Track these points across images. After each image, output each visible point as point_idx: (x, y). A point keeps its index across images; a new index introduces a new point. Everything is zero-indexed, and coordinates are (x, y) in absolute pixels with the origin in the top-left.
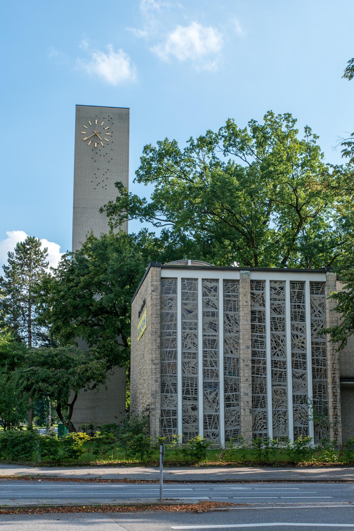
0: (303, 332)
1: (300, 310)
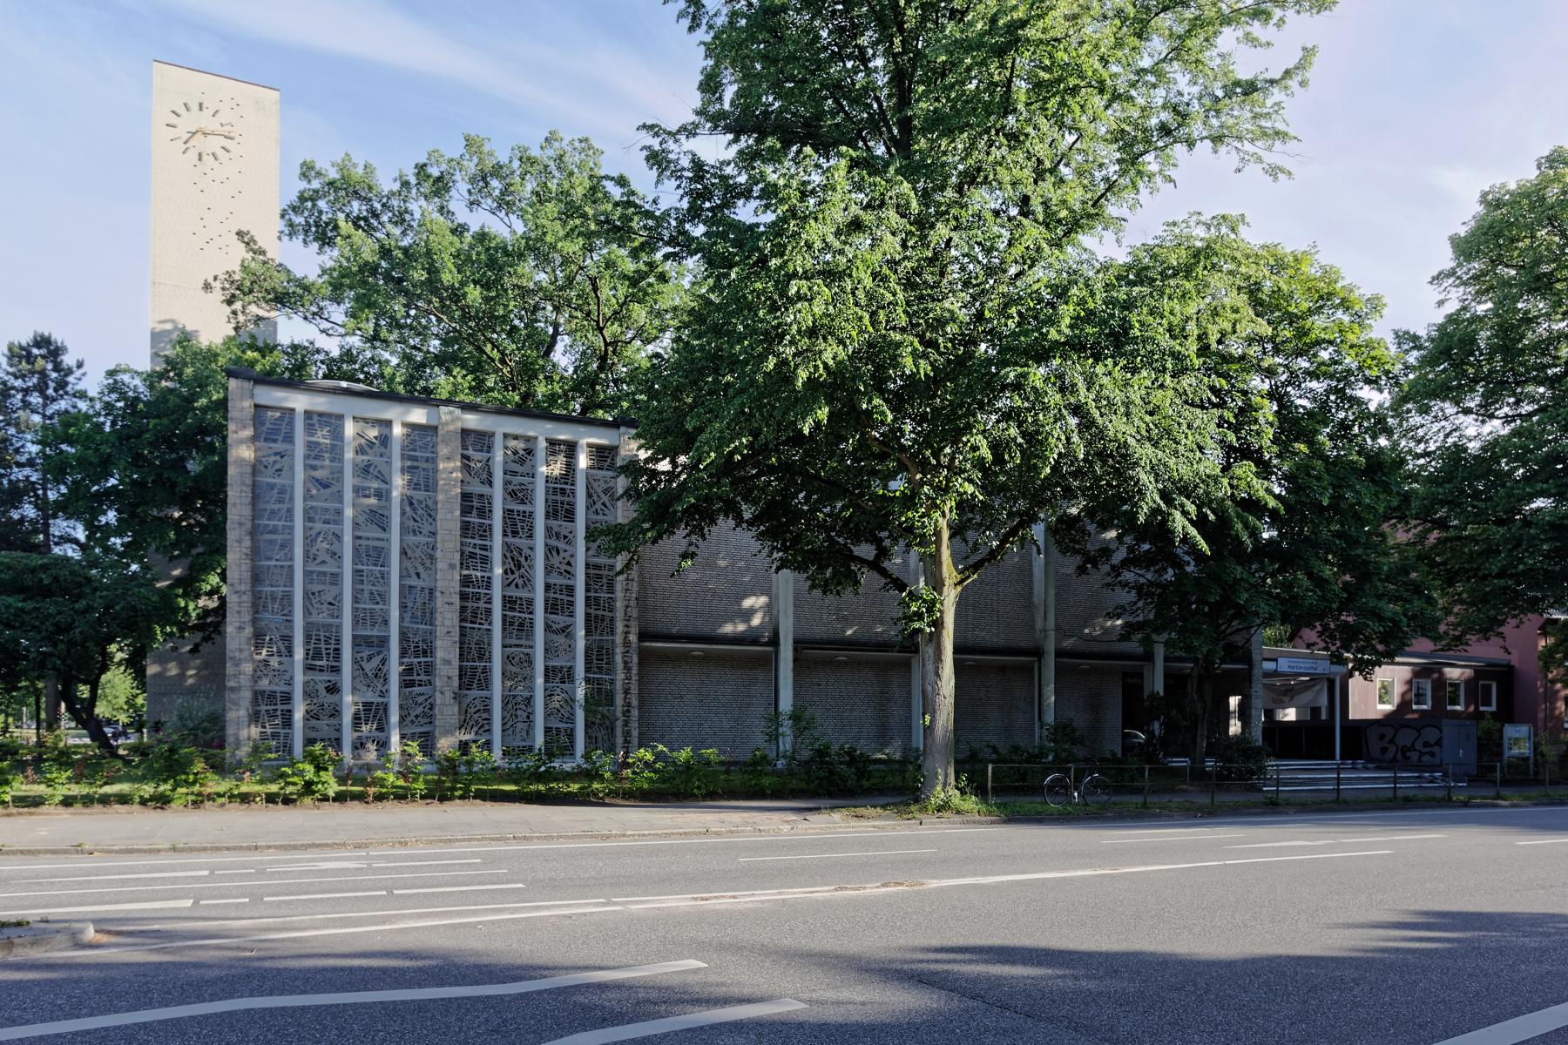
1: (566, 499)
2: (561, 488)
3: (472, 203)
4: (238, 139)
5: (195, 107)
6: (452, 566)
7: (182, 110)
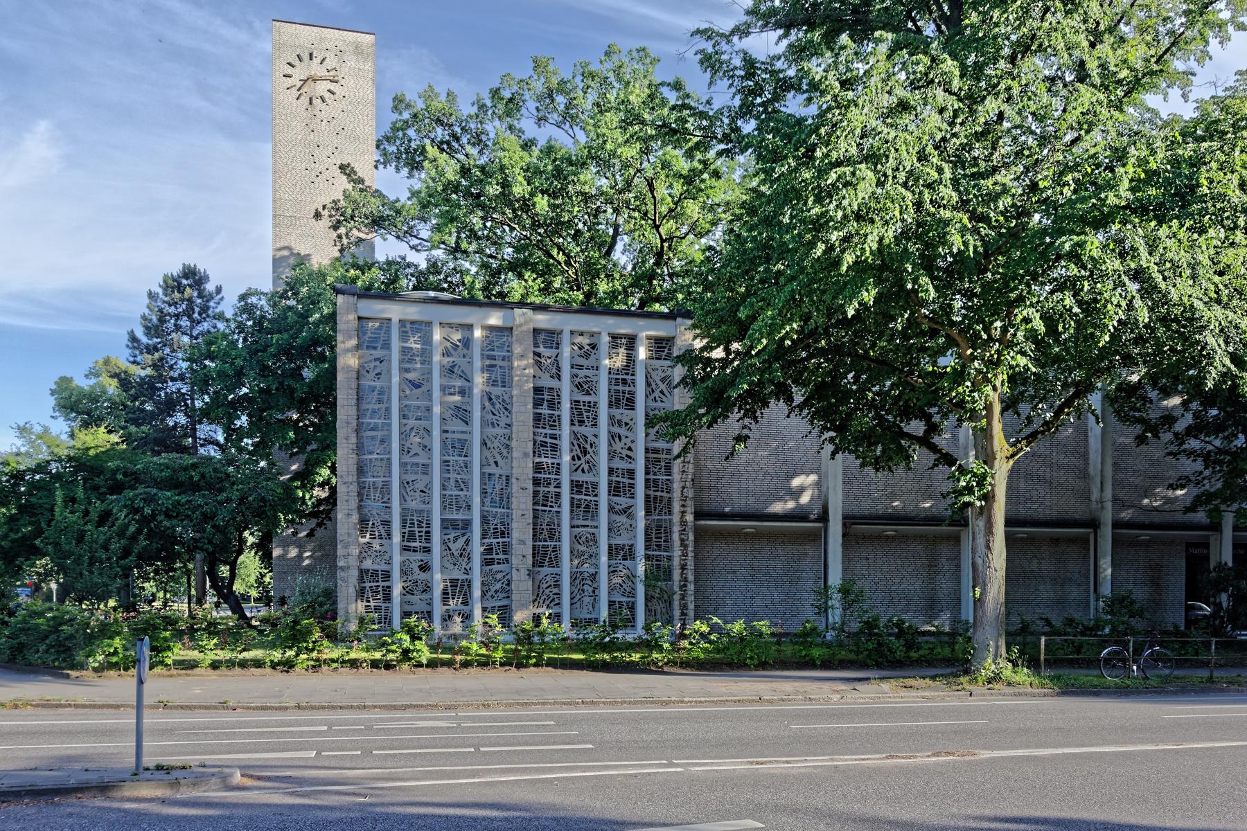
0: (630, 429)
2: (623, 377)
3: (540, 120)
4: (342, 82)
5: (306, 57)
6: (526, 455)
7: (296, 62)
